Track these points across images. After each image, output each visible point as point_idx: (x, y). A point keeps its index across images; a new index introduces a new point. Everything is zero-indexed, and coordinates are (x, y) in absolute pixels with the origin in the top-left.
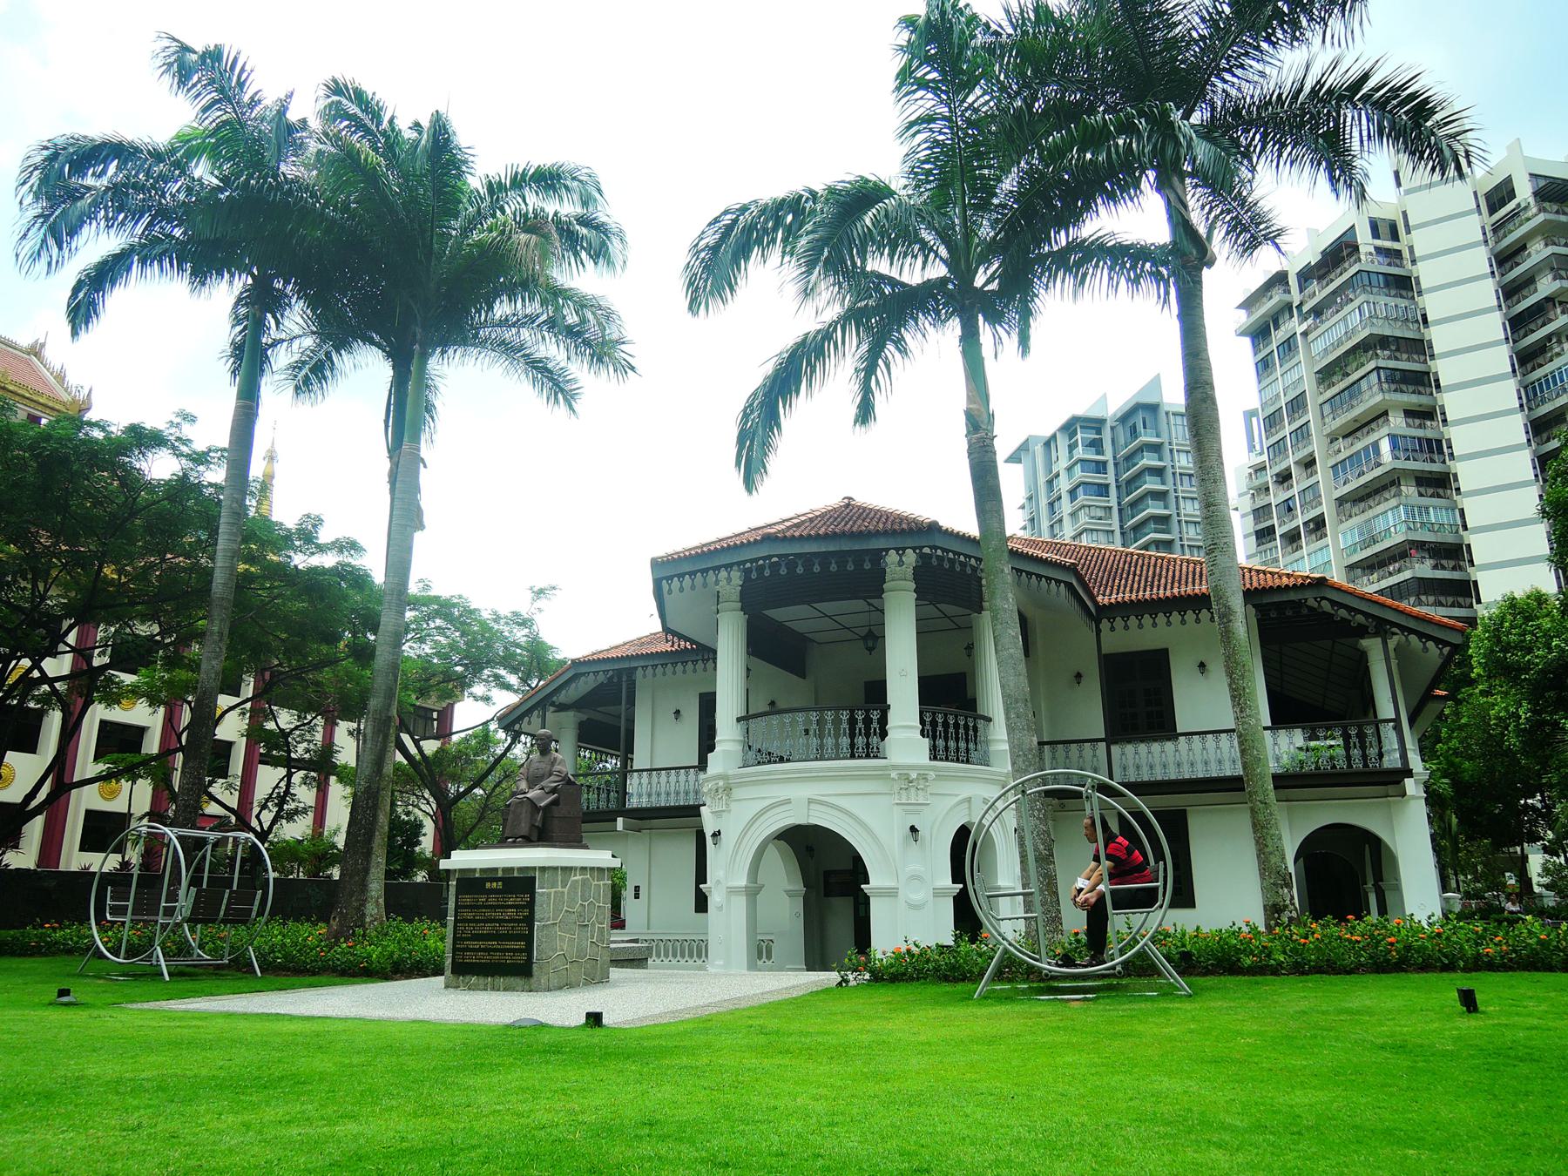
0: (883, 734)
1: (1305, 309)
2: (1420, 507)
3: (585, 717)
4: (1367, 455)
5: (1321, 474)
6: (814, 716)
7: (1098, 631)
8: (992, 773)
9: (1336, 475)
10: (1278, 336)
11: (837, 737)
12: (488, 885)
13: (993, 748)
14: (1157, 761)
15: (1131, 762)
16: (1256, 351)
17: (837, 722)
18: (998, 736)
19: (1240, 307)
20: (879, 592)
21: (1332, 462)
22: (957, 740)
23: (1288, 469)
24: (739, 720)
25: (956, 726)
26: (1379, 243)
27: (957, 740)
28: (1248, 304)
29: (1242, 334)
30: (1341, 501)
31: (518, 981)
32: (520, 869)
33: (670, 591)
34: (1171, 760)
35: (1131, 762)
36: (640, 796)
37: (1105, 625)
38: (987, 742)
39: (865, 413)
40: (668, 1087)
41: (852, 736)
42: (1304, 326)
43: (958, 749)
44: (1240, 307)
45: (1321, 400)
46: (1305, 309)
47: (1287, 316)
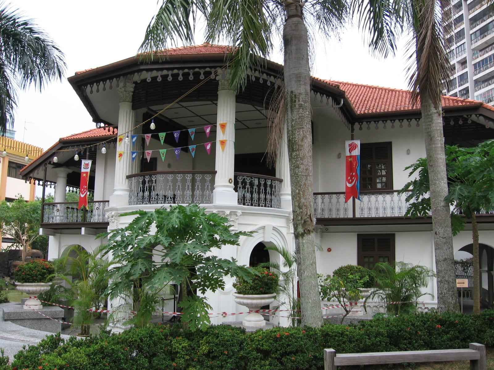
0: (213, 188)
2: (369, 178)
3: (70, 171)
4: (487, 62)
5: (469, 69)
6: (189, 177)
7: (353, 130)
8: (282, 212)
9: (475, 68)
11: (183, 190)
13: (283, 197)
14: (381, 206)
17: (184, 181)
18: (286, 191)
21: (473, 63)
22: (259, 193)
24: (128, 177)
25: (265, 185)
27: (259, 193)
30: (476, 82)
33: (92, 92)
34: (388, 205)
36: (99, 215)
37: (357, 126)
38: (280, 195)
41: (193, 190)
43: (259, 199)
45: (471, 32)
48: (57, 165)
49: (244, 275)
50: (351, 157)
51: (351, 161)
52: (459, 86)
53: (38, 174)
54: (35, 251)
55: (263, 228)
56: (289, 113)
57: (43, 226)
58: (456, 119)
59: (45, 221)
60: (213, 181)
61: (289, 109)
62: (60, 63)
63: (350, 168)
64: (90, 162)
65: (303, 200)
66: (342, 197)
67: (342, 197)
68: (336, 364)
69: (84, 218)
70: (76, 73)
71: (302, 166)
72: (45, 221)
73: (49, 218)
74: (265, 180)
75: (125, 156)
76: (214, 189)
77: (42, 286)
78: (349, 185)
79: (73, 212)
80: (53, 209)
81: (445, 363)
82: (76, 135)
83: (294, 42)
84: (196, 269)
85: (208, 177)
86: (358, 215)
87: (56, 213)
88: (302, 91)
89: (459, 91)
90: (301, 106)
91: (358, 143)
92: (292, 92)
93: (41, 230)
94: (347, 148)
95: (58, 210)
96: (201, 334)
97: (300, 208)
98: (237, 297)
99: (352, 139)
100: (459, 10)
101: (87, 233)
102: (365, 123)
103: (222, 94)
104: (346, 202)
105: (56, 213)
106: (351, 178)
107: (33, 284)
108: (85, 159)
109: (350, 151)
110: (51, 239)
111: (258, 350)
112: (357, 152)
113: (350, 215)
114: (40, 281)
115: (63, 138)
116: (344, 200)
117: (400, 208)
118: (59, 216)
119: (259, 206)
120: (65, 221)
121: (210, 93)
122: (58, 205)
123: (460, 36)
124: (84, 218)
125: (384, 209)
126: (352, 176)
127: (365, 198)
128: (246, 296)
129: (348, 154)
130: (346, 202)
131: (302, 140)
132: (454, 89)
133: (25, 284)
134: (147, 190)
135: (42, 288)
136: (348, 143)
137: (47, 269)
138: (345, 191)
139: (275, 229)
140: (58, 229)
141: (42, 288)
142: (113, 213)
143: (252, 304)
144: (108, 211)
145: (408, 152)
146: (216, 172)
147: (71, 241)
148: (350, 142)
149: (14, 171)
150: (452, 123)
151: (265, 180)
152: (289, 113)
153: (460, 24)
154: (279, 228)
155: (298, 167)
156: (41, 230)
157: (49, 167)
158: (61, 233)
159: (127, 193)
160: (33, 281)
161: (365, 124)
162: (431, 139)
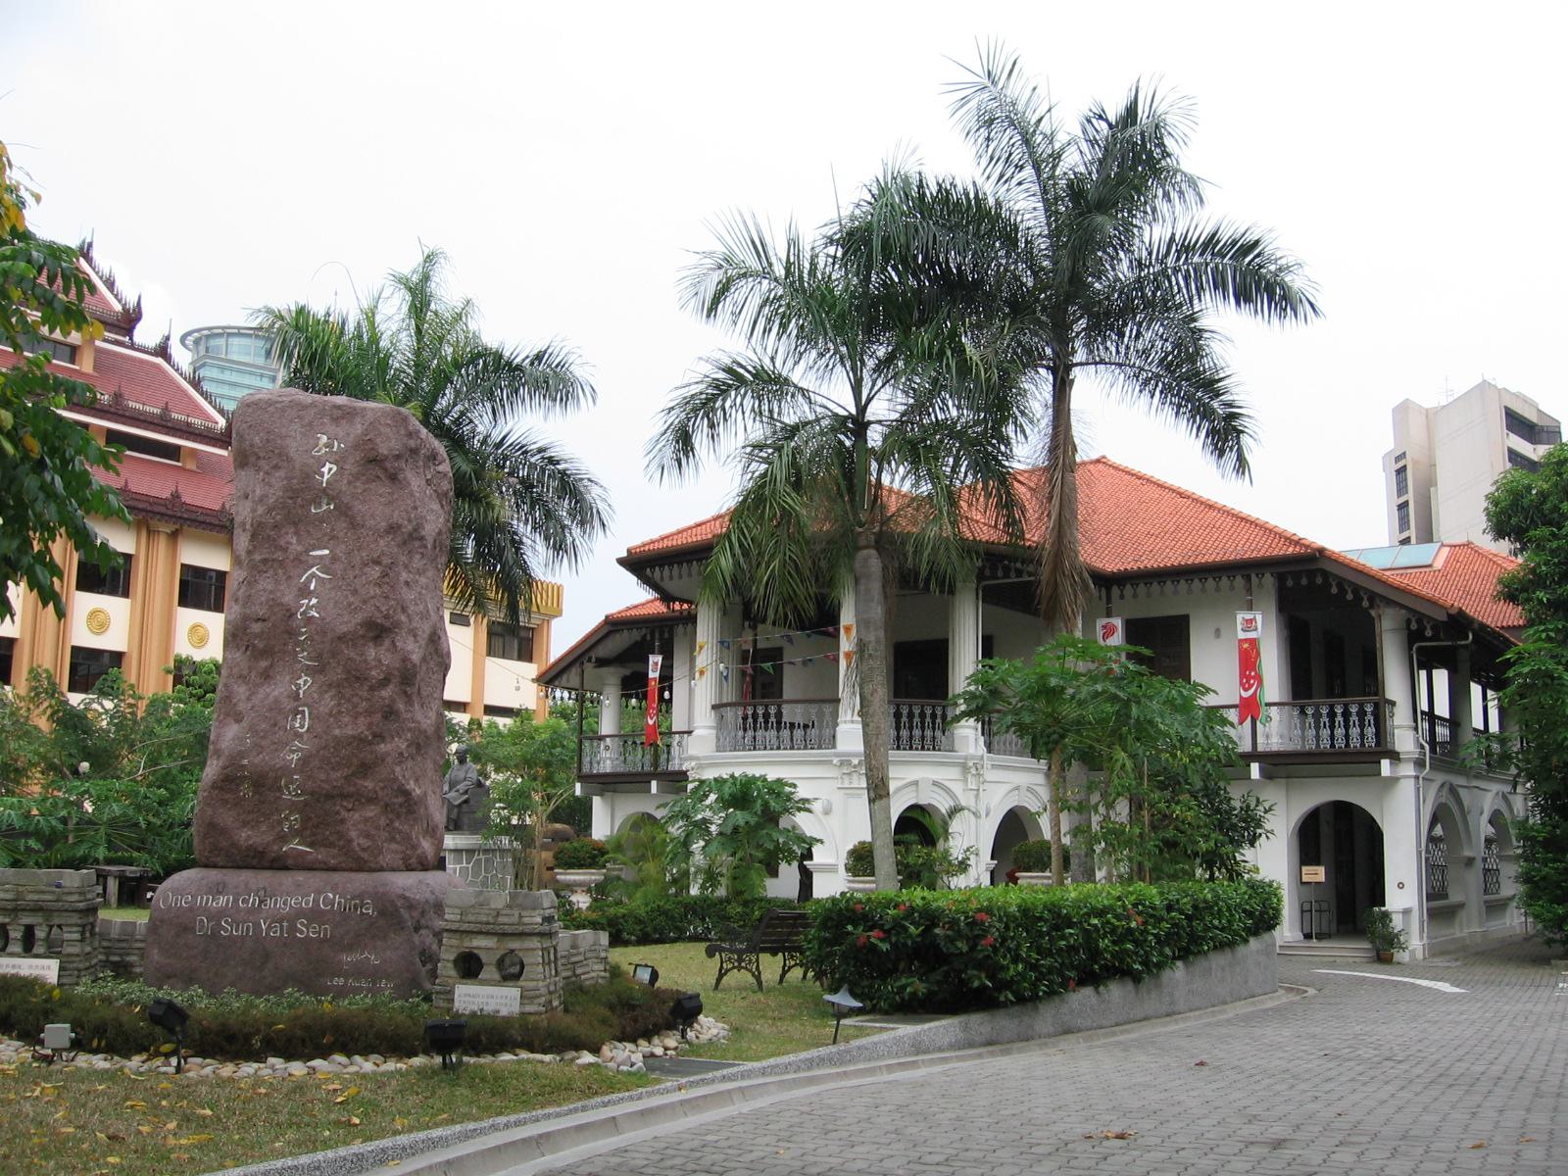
3: (627, 672)
7: (1109, 600)
22: (911, 729)
24: (714, 707)
27: (911, 729)
37: (1115, 590)
43: (911, 737)
48: (602, 663)
49: (1073, 891)
53: (568, 681)
54: (558, 826)
55: (916, 783)
57: (583, 778)
58: (1297, 576)
59: (586, 769)
60: (835, 715)
62: (601, 505)
64: (659, 659)
65: (873, 762)
69: (656, 763)
71: (871, 724)
72: (586, 769)
73: (591, 763)
74: (934, 707)
75: (708, 674)
76: (837, 725)
77: (592, 874)
78: (1245, 695)
79: (634, 749)
80: (599, 746)
82: (636, 607)
83: (863, 581)
85: (827, 709)
87: (604, 754)
88: (872, 638)
90: (870, 655)
91: (1118, 622)
93: (578, 786)
94: (1100, 632)
95: (607, 748)
96: (755, 900)
97: (871, 770)
98: (850, 881)
99: (1109, 615)
101: (661, 790)
102: (1128, 586)
105: (604, 754)
108: (653, 653)
109: (1105, 637)
110: (597, 801)
114: (590, 866)
115: (612, 615)
118: (610, 758)
119: (911, 748)
120: (621, 769)
122: (608, 739)
124: (656, 763)
129: (1242, 635)
131: (872, 695)
135: (593, 877)
136: (1101, 622)
137: (599, 850)
138: (1237, 702)
139: (935, 783)
140: (610, 784)
141: (593, 877)
142: (693, 764)
144: (686, 759)
146: (839, 700)
147: (632, 806)
148: (1105, 621)
149: (498, 642)
150: (1290, 583)
151: (934, 707)
154: (946, 783)
156: (578, 786)
157: (589, 668)
158: (615, 791)
159: (714, 732)
160: (581, 866)
161: (1128, 590)
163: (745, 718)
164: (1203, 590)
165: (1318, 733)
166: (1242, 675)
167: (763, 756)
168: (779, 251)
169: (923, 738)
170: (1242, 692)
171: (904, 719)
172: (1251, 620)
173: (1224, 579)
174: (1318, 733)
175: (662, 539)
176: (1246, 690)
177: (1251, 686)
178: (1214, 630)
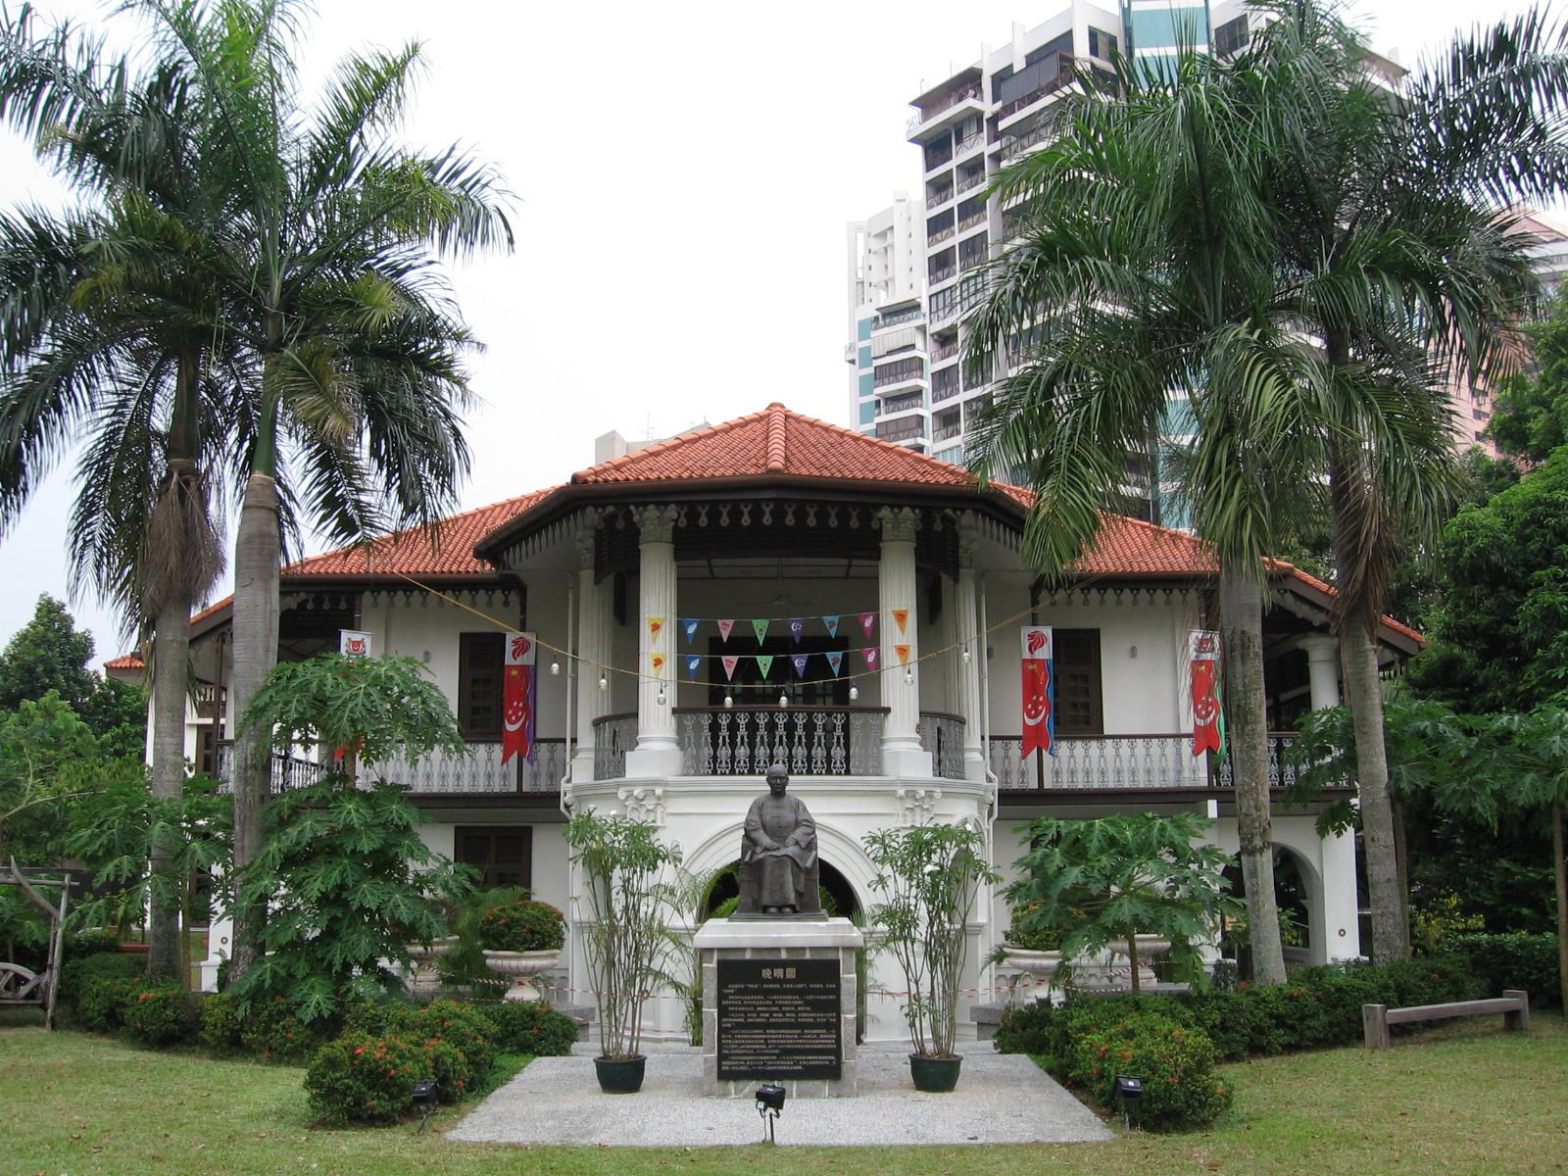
1: (1002, 125)
10: (961, 155)
12: (766, 973)
15: (1095, 766)
16: (929, 167)
19: (915, 103)
20: (876, 555)
23: (953, 328)
26: (1096, 61)
28: (928, 103)
29: (914, 140)
31: (826, 1087)
32: (789, 949)
35: (1095, 766)
39: (453, 149)
40: (397, 963)
42: (996, 146)
43: (733, 757)
44: (915, 103)
46: (1002, 125)
47: (975, 129)
50: (1033, 661)
51: (1033, 671)
52: (965, 390)
56: (1238, 664)
61: (1238, 658)
63: (1031, 686)
66: (1015, 745)
67: (1015, 745)
68: (1389, 1022)
70: (575, 478)
78: (1031, 722)
81: (1454, 1019)
84: (270, 911)
86: (1048, 785)
89: (965, 403)
91: (1047, 632)
92: (1243, 632)
94: (1026, 643)
99: (1034, 624)
100: (974, 179)
103: (887, 548)
104: (1024, 757)
106: (1035, 707)
107: (545, 952)
111: (1271, 1016)
112: (1045, 653)
113: (1033, 784)
116: (1019, 753)
117: (1149, 772)
121: (868, 547)
123: (974, 252)
125: (1087, 773)
126: (1035, 704)
127: (1063, 747)
128: (1048, 953)
129: (1027, 655)
130: (1024, 757)
132: (951, 395)
133: (526, 953)
134: (742, 743)
136: (1026, 631)
138: (1021, 733)
143: (1042, 968)
145: (1133, 652)
148: (1032, 629)
152: (1238, 664)
153: (976, 217)
155: (1255, 748)
162: (1365, 691)
163: (715, 728)
164: (1119, 602)
165: (809, 752)
166: (1026, 700)
167: (842, 783)
168: (101, 77)
169: (809, 758)
170: (1198, 721)
171: (724, 732)
172: (359, 642)
173: (1143, 592)
174: (809, 752)
175: (681, 443)
176: (1204, 718)
177: (1208, 714)
178: (1127, 647)
